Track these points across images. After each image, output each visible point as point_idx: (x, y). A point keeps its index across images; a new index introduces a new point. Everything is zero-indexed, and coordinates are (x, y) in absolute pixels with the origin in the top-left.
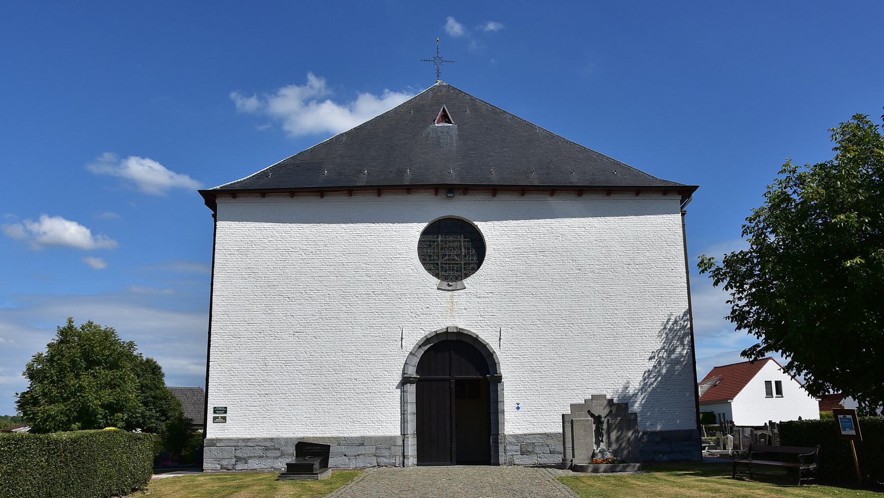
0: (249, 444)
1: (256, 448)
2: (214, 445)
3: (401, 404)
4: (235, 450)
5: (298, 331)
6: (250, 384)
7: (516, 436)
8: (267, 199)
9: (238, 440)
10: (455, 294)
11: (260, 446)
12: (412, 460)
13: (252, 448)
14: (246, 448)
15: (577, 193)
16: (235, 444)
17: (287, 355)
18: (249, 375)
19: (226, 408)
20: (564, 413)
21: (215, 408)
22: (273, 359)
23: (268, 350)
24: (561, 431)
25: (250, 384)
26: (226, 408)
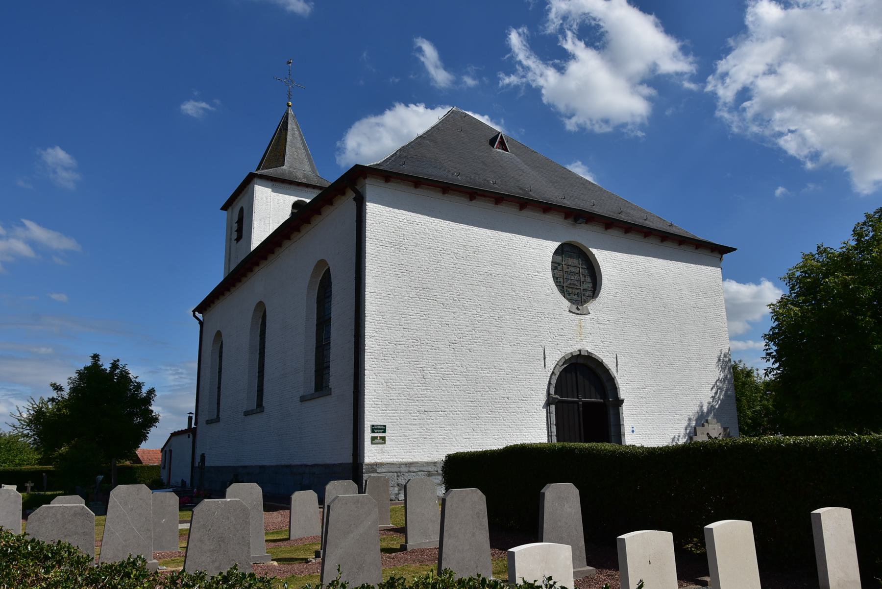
1: (419, 473)
4: (398, 476)
11: (424, 471)
13: (414, 474)
16: (398, 469)
17: (445, 367)
18: (408, 388)
19: (385, 426)
21: (373, 426)
23: (426, 361)
26: (385, 426)
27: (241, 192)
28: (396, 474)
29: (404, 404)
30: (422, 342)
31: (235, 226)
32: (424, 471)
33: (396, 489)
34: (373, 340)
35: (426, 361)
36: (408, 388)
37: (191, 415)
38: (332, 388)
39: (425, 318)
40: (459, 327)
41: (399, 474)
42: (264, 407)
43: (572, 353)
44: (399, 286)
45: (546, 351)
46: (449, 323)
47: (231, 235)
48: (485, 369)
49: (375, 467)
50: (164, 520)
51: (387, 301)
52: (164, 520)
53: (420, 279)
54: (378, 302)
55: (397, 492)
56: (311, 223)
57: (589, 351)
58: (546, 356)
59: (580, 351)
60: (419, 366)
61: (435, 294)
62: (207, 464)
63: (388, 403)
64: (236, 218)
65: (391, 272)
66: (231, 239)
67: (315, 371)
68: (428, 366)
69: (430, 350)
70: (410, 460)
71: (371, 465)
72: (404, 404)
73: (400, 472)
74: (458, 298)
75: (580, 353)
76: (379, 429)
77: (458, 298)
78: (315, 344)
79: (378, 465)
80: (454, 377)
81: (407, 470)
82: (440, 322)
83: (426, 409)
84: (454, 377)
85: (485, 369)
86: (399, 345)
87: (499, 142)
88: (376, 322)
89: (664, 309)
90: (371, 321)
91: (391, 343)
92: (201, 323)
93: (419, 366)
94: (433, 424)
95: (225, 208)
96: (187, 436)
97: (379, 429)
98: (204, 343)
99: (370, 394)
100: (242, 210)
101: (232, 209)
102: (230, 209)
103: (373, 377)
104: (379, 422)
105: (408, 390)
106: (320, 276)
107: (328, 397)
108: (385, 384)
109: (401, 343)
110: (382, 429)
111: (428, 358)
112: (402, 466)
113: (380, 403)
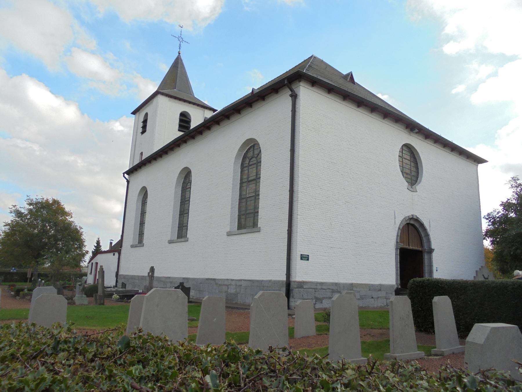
0: (324, 287)
1: (327, 290)
2: (301, 287)
3: (396, 263)
4: (315, 291)
5: (348, 201)
6: (322, 238)
7: (157, 277)
8: (314, 89)
9: (317, 283)
10: (414, 194)
11: (329, 289)
12: (361, 303)
13: (324, 290)
14: (322, 290)
15: (406, 125)
16: (315, 287)
17: (342, 218)
18: (322, 231)
19: (308, 256)
20: (307, 262)
21: (301, 255)
22: (335, 220)
23: (332, 212)
24: (284, 278)
25: (322, 238)
26: (308, 256)
27: (147, 103)
28: (314, 290)
29: (320, 241)
30: (330, 199)
31: (141, 125)
32: (329, 289)
33: (314, 300)
34: (303, 195)
35: (332, 212)
36: (322, 231)
37: (111, 241)
38: (261, 227)
39: (332, 183)
40: (351, 192)
41: (316, 290)
42: (188, 238)
43: (409, 216)
44: (318, 159)
45: (396, 214)
46: (345, 188)
47: (137, 130)
48: (364, 222)
49: (302, 284)
50: (215, 319)
51: (311, 168)
52: (215, 319)
53: (330, 156)
54: (306, 169)
55: (314, 303)
56: (241, 113)
57: (418, 216)
58: (396, 217)
59: (413, 215)
60: (328, 215)
61: (338, 167)
62: (156, 275)
63: (310, 240)
64: (142, 119)
65: (314, 149)
66: (137, 132)
67: (238, 215)
68: (333, 216)
69: (334, 205)
70: (322, 281)
71: (299, 282)
72: (320, 241)
73: (317, 289)
74: (350, 172)
75: (413, 216)
76: (305, 257)
77: (350, 172)
78: (238, 197)
79: (304, 283)
80: (347, 225)
81: (320, 288)
82: (340, 187)
83: (332, 246)
84: (347, 225)
85: (364, 222)
86: (317, 200)
87: (350, 77)
88: (305, 182)
89: (452, 194)
90: (302, 181)
91: (313, 198)
92: (128, 182)
93: (328, 215)
94: (335, 257)
95: (134, 113)
96: (113, 255)
97: (305, 257)
98: (129, 194)
99: (300, 232)
100: (146, 115)
101: (139, 114)
102: (137, 114)
103: (302, 220)
104: (305, 253)
105: (322, 231)
106: (245, 150)
107: (256, 233)
108: (309, 226)
109: (318, 198)
110: (307, 258)
111: (333, 211)
112: (318, 284)
113: (306, 239)
